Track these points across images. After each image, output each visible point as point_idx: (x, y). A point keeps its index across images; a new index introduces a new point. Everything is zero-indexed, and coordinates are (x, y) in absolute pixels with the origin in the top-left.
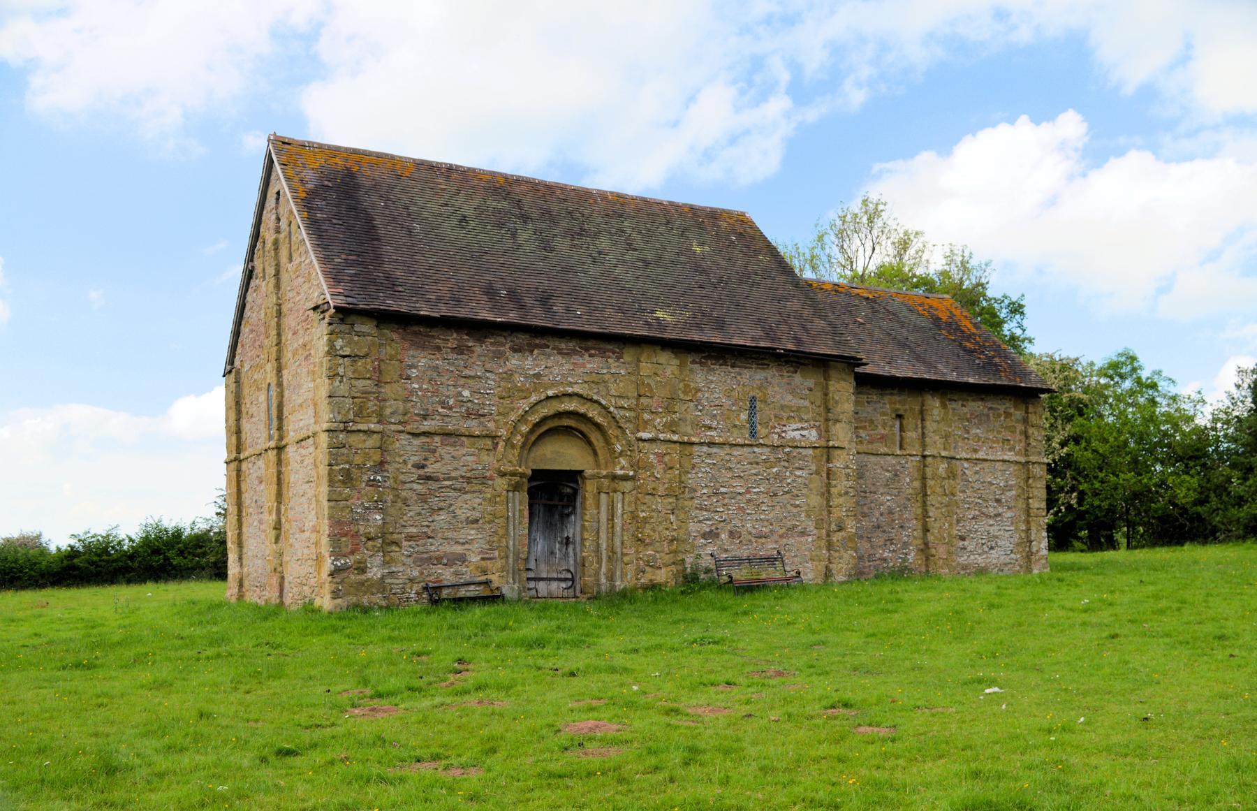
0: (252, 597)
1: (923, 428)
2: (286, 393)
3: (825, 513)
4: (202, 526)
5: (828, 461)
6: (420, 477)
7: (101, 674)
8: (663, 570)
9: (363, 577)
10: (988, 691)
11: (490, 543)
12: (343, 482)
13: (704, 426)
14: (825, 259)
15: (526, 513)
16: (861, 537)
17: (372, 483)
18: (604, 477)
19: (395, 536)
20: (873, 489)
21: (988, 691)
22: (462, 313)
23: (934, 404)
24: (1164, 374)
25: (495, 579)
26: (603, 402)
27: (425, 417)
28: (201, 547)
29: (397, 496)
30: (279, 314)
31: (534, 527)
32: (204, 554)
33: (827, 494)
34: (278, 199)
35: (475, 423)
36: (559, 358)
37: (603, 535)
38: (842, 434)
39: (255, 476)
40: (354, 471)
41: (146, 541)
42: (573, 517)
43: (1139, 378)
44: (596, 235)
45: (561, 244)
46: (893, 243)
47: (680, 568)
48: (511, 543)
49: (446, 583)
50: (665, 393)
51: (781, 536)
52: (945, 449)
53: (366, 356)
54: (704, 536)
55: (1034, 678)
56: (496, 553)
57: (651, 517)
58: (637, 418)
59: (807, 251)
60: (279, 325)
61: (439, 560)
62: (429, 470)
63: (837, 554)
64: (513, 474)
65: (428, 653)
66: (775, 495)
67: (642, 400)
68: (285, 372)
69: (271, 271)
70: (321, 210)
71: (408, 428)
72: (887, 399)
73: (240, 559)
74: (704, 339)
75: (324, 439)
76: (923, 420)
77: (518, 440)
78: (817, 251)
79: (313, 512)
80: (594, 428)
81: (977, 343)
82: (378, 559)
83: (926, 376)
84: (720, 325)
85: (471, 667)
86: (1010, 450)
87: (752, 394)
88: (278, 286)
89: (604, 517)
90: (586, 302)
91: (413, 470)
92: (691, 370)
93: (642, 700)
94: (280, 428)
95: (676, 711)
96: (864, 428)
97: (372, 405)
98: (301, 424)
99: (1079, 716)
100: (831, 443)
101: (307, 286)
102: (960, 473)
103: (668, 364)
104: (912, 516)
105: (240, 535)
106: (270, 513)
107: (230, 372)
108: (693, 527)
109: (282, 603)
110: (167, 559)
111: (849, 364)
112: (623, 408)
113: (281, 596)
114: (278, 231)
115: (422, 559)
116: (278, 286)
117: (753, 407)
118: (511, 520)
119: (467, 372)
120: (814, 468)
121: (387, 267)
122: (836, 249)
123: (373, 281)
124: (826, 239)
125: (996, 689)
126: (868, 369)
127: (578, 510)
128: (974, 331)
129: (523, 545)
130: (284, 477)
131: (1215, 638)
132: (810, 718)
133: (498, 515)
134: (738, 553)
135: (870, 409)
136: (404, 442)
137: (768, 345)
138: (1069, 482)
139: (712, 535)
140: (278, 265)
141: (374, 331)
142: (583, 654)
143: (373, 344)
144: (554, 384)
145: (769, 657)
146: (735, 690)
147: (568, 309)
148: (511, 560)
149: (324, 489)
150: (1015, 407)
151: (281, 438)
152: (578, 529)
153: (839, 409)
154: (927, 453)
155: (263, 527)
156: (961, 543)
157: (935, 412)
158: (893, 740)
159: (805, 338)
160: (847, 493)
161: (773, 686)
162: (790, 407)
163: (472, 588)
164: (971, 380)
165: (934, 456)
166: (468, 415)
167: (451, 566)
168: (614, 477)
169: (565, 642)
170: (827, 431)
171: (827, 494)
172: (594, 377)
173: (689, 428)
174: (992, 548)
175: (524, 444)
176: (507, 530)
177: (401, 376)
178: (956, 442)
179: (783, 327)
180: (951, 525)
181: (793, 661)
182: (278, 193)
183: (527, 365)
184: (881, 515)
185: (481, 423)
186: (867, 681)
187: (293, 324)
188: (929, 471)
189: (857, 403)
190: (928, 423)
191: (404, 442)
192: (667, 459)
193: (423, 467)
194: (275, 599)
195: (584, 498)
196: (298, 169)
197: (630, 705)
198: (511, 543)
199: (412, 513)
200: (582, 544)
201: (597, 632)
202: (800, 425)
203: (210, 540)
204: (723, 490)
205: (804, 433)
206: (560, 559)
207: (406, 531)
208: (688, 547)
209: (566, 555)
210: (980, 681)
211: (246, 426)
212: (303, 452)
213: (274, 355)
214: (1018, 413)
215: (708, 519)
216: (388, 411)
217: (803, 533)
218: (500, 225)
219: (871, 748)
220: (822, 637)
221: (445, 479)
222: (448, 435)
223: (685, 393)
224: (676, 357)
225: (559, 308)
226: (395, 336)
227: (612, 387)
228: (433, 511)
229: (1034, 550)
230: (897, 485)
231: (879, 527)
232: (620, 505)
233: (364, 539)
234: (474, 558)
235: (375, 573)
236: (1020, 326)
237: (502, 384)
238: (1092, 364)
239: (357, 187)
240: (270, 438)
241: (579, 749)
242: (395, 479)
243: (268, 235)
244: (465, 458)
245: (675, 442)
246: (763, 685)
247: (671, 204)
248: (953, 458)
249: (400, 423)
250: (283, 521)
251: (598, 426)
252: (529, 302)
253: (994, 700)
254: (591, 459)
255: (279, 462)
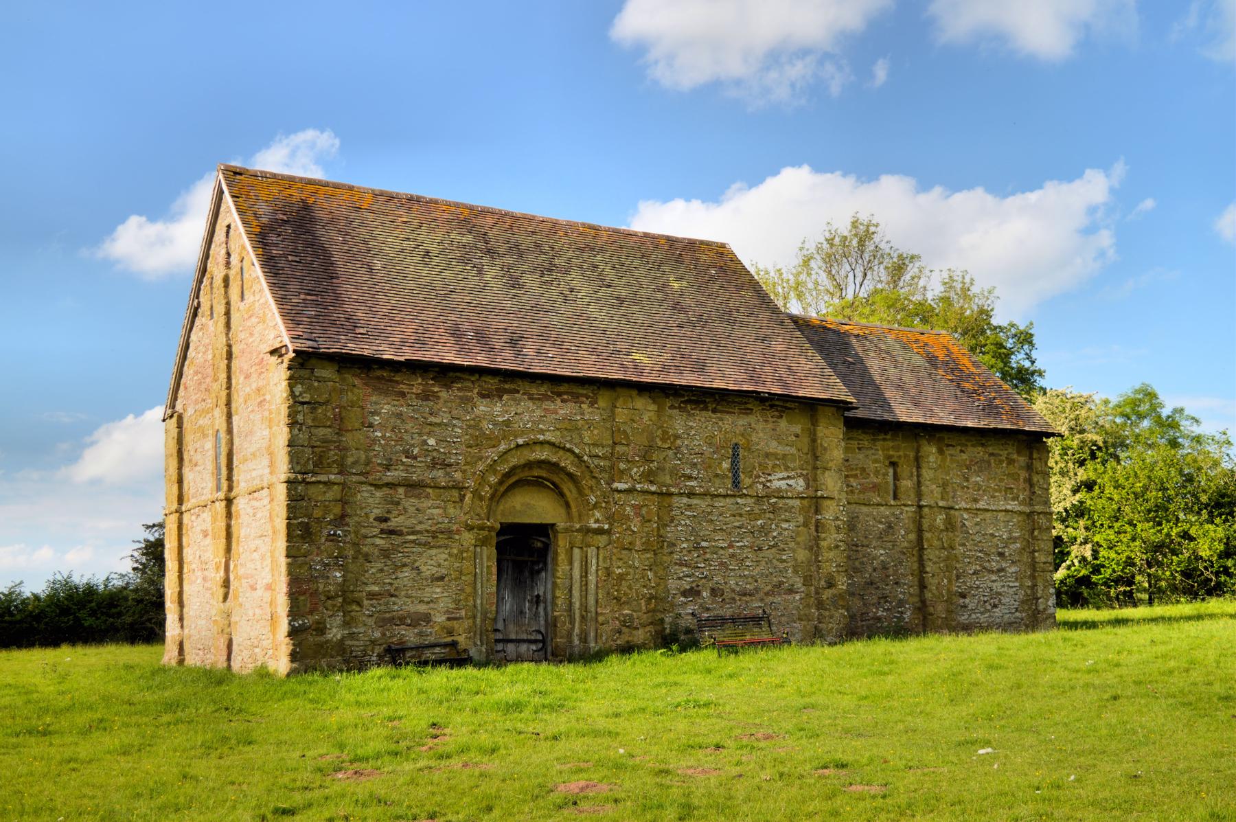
0: (192, 660)
1: (919, 476)
2: (236, 441)
3: (813, 569)
4: (117, 583)
5: (817, 512)
6: (382, 532)
7: (56, 740)
8: (640, 632)
9: (322, 639)
10: (981, 752)
11: (457, 602)
12: (302, 537)
13: (684, 476)
14: (810, 286)
15: (494, 570)
16: (852, 594)
17: (332, 538)
18: (577, 531)
19: (356, 595)
20: (865, 542)
21: (981, 752)
22: (428, 355)
23: (930, 451)
24: (1186, 413)
25: (462, 640)
26: (577, 451)
27: (388, 468)
28: (116, 606)
29: (358, 552)
30: (230, 356)
31: (502, 585)
32: (119, 614)
33: (814, 547)
34: (228, 232)
35: (440, 473)
36: (530, 404)
37: (576, 593)
38: (831, 483)
39: (199, 528)
40: (314, 528)
41: (53, 599)
42: (543, 574)
43: (1160, 417)
44: (567, 271)
45: (531, 281)
46: (886, 268)
47: (659, 628)
48: (479, 602)
49: (409, 645)
50: (643, 440)
51: (767, 594)
52: (942, 499)
53: (326, 403)
54: (685, 593)
55: (1030, 739)
56: (463, 613)
57: (628, 574)
58: (612, 467)
59: (791, 277)
60: (229, 367)
61: (402, 620)
62: (395, 522)
63: (827, 613)
64: (481, 528)
65: (400, 718)
66: (760, 549)
67: (618, 448)
68: (235, 419)
69: (220, 309)
70: (276, 245)
71: (371, 478)
72: (879, 444)
73: (181, 619)
74: (684, 382)
75: (281, 490)
76: (919, 467)
77: (486, 491)
78: (803, 277)
79: (267, 569)
80: (566, 478)
81: (977, 383)
82: (338, 620)
83: (921, 420)
84: (700, 367)
85: (447, 731)
86: (1013, 499)
87: (734, 441)
88: (228, 325)
89: (576, 573)
90: (558, 344)
91: (376, 524)
92: (670, 417)
93: (631, 762)
94: (230, 478)
95: (667, 772)
96: (855, 476)
97: (333, 454)
98: (254, 474)
99: (1069, 775)
100: (819, 493)
101: (260, 327)
102: (959, 524)
103: (646, 408)
104: (908, 571)
105: (180, 594)
106: (217, 569)
107: (171, 417)
108: (672, 584)
109: (229, 667)
110: (77, 619)
111: (838, 408)
112: (597, 456)
113: (229, 659)
114: (228, 264)
115: (384, 620)
116: (228, 325)
117: (735, 456)
118: (479, 577)
119: (432, 419)
120: (801, 519)
121: (348, 308)
122: (823, 275)
123: (333, 323)
124: (813, 264)
125: (990, 750)
126: (859, 414)
127: (550, 566)
128: (975, 370)
129: (491, 604)
130: (234, 530)
131: (1220, 698)
132: (801, 777)
133: (465, 571)
134: (721, 612)
135: (861, 456)
136: (365, 494)
137: (751, 388)
138: (1081, 534)
139: (693, 592)
140: (228, 303)
141: (335, 377)
142: (563, 719)
143: (334, 389)
144: (523, 433)
145: (758, 721)
146: (725, 752)
147: (539, 352)
148: (478, 620)
149: (282, 544)
150: (1019, 453)
151: (230, 489)
152: (549, 586)
153: (827, 457)
154: (923, 503)
155: (208, 585)
156: (962, 601)
157: (932, 459)
158: (884, 797)
159: (790, 380)
160: (837, 547)
161: (762, 749)
162: (775, 455)
163: (437, 650)
164: (970, 424)
165: (930, 507)
166: (434, 465)
167: (415, 627)
168: (589, 531)
169: (544, 706)
170: (815, 480)
171: (814, 547)
172: (566, 425)
173: (668, 477)
174: (995, 606)
175: (493, 496)
176: (475, 588)
177: (363, 424)
178: (955, 491)
179: (767, 369)
180: (950, 581)
181: (783, 724)
182: (229, 227)
183: (492, 411)
184: (875, 570)
185: (447, 474)
186: (858, 743)
187: (245, 367)
188: (926, 524)
189: (847, 450)
190: (924, 472)
191: (365, 494)
192: (644, 511)
193: (386, 520)
194: (221, 664)
195: (556, 553)
196: (251, 202)
197: (619, 767)
198: (479, 602)
199: (373, 570)
200: (554, 604)
201: (575, 695)
202: (785, 474)
203: (126, 599)
204: (704, 544)
205: (791, 482)
206: (530, 619)
207: (368, 589)
208: (667, 606)
209: (537, 615)
210: (974, 742)
211: (188, 475)
212: (255, 503)
213: (223, 400)
214: (1021, 459)
215: (687, 576)
216: (350, 460)
217: (791, 591)
218: (464, 260)
219: (861, 805)
220: (812, 700)
221: (409, 534)
222: (414, 487)
223: (664, 440)
224: (654, 402)
225: (529, 350)
226: (357, 381)
227: (586, 434)
228: (396, 568)
229: (1041, 607)
230: (890, 538)
231: (872, 583)
232: (594, 561)
233: (323, 598)
234: (440, 619)
235: (335, 633)
236: (1029, 357)
237: (470, 431)
238: (1106, 402)
239: (312, 220)
240: (218, 489)
241: (572, 807)
242: (356, 533)
243: (216, 270)
244: (430, 511)
245: (653, 493)
246: (752, 747)
247: (646, 235)
248: (952, 508)
249: (362, 474)
250: (232, 578)
251: (571, 476)
252: (499, 345)
253: (983, 760)
254: (563, 511)
255: (229, 515)
